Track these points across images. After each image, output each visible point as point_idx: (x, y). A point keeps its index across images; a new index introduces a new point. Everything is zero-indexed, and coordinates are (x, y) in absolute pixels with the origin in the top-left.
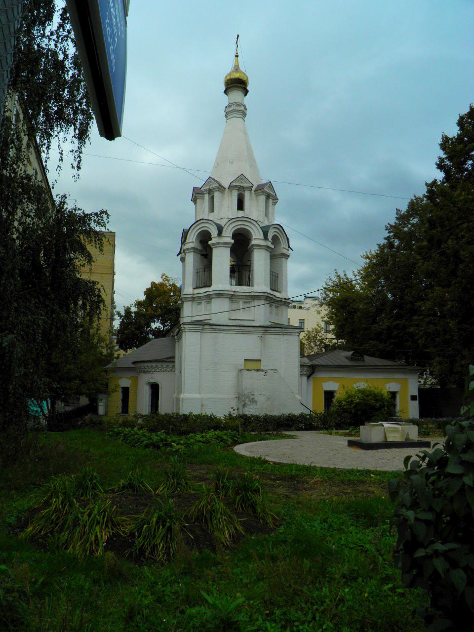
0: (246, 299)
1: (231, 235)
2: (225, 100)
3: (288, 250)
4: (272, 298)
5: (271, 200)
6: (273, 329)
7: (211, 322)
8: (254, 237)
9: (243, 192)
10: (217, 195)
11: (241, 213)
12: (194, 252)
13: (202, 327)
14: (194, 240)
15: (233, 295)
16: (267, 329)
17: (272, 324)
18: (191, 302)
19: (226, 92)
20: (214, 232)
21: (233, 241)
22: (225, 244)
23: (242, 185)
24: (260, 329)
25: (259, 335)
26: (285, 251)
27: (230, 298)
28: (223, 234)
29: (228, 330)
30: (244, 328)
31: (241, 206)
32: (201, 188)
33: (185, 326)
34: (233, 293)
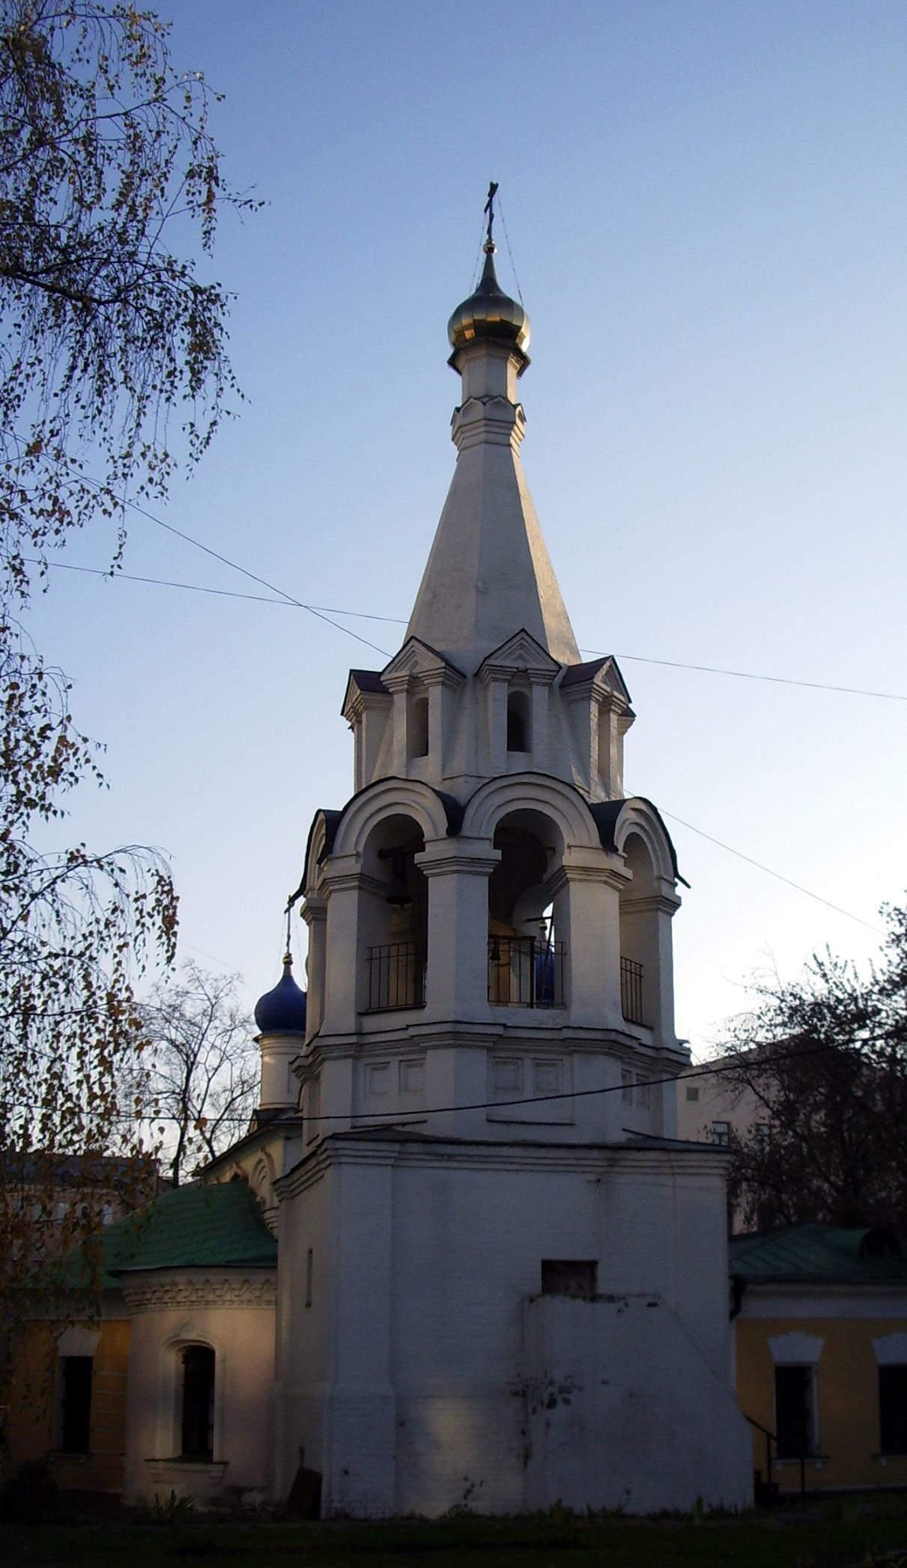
0: (545, 1052)
1: (492, 836)
2: (452, 389)
3: (676, 884)
4: (632, 1048)
7: (426, 1130)
8: (567, 839)
9: (525, 690)
10: (435, 695)
11: (519, 762)
13: (397, 1147)
14: (361, 849)
17: (630, 1135)
18: (350, 1061)
19: (453, 362)
21: (498, 854)
23: (521, 665)
24: (595, 1154)
26: (665, 890)
27: (489, 1049)
28: (467, 829)
29: (451, 1157)
30: (542, 1152)
31: (518, 737)
32: (381, 674)
33: (339, 1144)
34: (499, 1030)
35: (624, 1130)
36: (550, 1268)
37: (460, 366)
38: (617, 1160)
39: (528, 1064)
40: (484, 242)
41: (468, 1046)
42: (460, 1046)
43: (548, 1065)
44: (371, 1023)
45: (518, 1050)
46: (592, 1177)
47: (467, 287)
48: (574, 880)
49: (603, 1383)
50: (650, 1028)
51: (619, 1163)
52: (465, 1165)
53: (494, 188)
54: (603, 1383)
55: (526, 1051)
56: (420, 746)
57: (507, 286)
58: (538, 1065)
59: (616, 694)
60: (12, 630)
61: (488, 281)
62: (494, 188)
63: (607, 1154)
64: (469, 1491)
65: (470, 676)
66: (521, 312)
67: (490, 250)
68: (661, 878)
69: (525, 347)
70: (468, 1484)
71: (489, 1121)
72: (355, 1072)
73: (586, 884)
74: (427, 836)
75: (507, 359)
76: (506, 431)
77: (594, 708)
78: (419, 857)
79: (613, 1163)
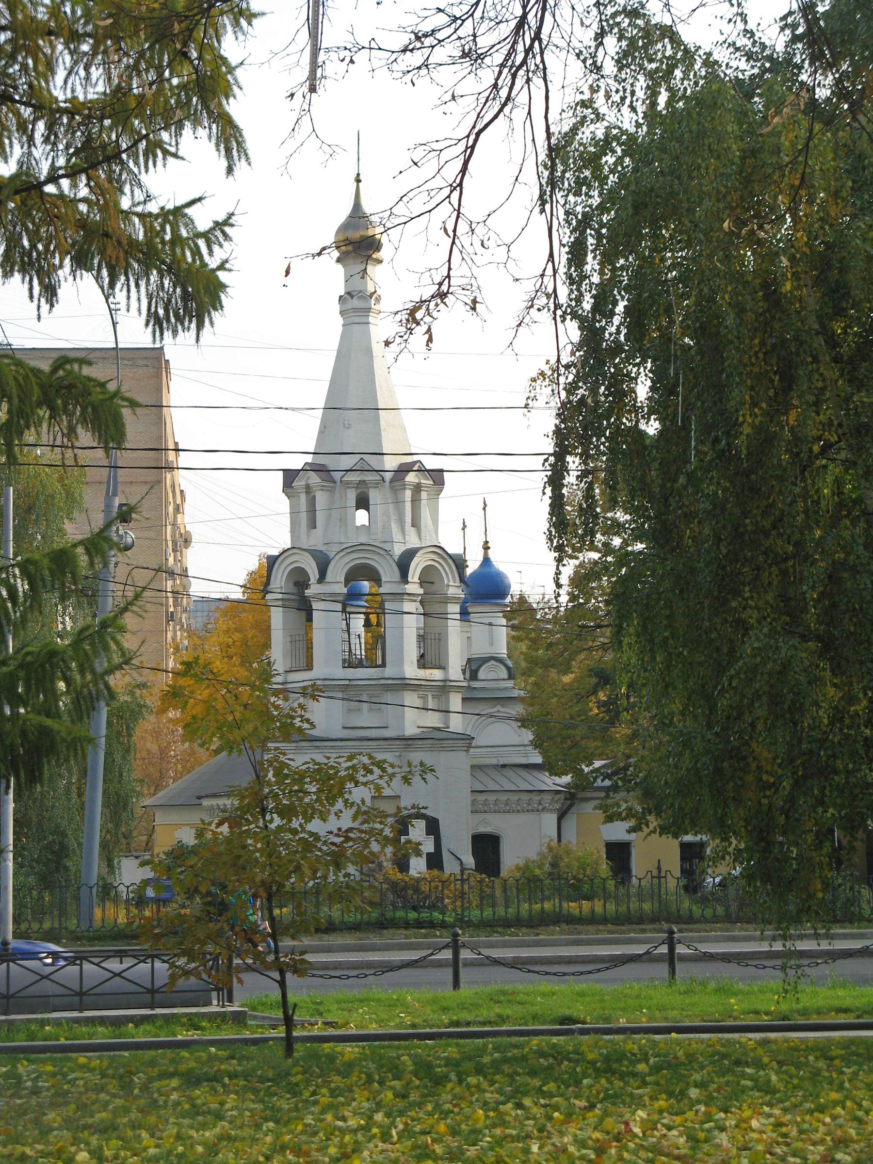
1: (343, 580)
5: (424, 495)
6: (420, 742)
16: (410, 742)
20: (314, 574)
22: (332, 598)
24: (398, 742)
25: (397, 754)
28: (329, 577)
30: (370, 743)
34: (347, 682)
46: (397, 754)
50: (444, 668)
56: (313, 525)
57: (367, 207)
61: (357, 205)
67: (358, 181)
68: (448, 586)
77: (408, 494)
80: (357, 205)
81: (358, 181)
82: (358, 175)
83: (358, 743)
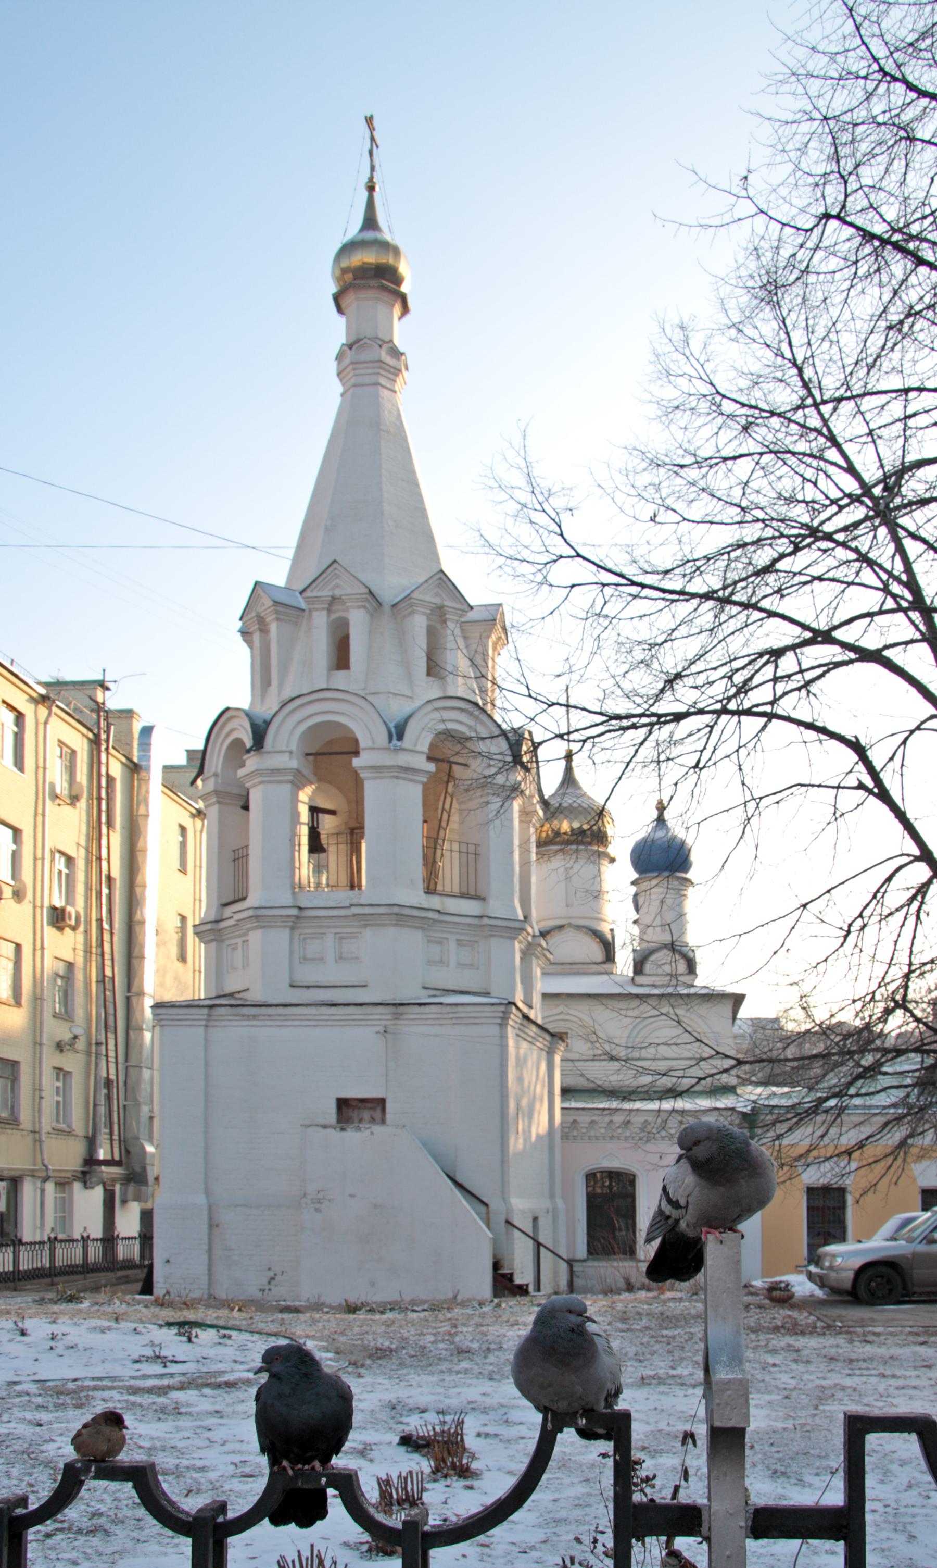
12: (219, 803)
14: (219, 770)
15: (435, 920)
24: (380, 1009)
29: (254, 1017)
30: (333, 1010)
35: (425, 988)
36: (343, 1104)
37: (343, 305)
38: (402, 1014)
39: (330, 940)
40: (366, 180)
41: (271, 927)
42: (265, 927)
43: (351, 938)
44: (228, 911)
45: (320, 927)
47: (353, 228)
48: (368, 778)
49: (352, 1196)
51: (405, 1017)
52: (268, 1023)
53: (369, 120)
54: (352, 1196)
55: (328, 927)
58: (429, 941)
59: (447, 603)
60: (615, 638)
61: (370, 222)
62: (369, 120)
63: (392, 1009)
64: (272, 1279)
65: (387, 608)
66: (396, 251)
67: (371, 188)
69: (404, 288)
70: (271, 1274)
71: (292, 986)
72: (291, 939)
73: (396, 781)
74: (362, 744)
75: (393, 306)
76: (391, 376)
78: (356, 762)
79: (397, 1017)
80: (370, 222)
81: (371, 188)
82: (371, 179)
83: (313, 1010)
